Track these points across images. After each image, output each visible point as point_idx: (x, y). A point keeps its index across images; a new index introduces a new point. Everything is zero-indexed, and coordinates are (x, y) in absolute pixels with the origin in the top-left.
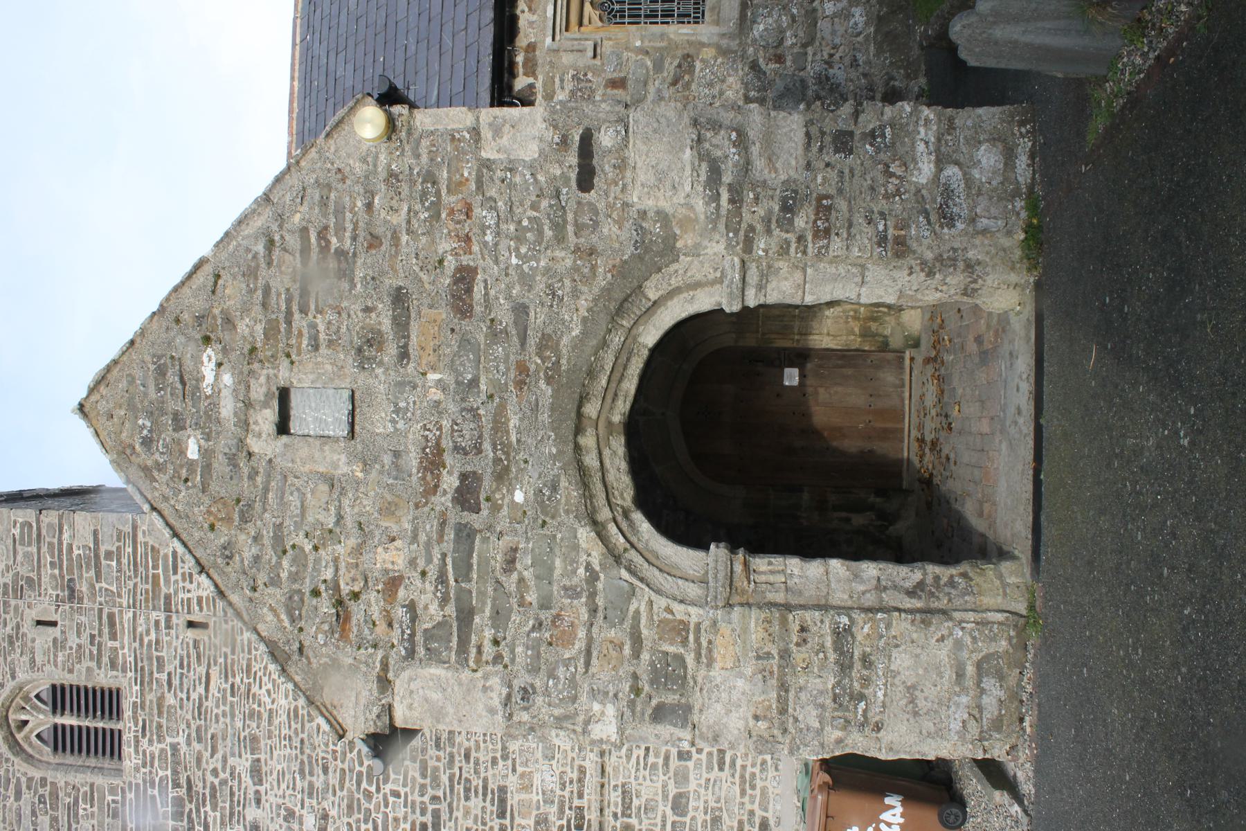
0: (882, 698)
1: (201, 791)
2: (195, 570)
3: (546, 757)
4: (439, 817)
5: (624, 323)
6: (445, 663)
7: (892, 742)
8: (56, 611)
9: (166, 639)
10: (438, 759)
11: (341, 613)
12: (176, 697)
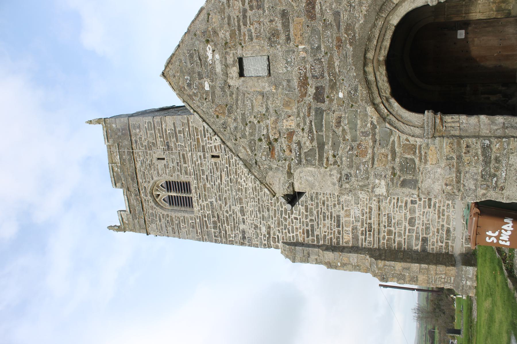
0: (504, 176)
1: (223, 219)
2: (213, 134)
3: (355, 203)
4: (313, 227)
5: (383, 15)
6: (314, 165)
7: (509, 195)
8: (164, 154)
9: (204, 162)
10: (312, 205)
11: (271, 147)
12: (210, 185)
